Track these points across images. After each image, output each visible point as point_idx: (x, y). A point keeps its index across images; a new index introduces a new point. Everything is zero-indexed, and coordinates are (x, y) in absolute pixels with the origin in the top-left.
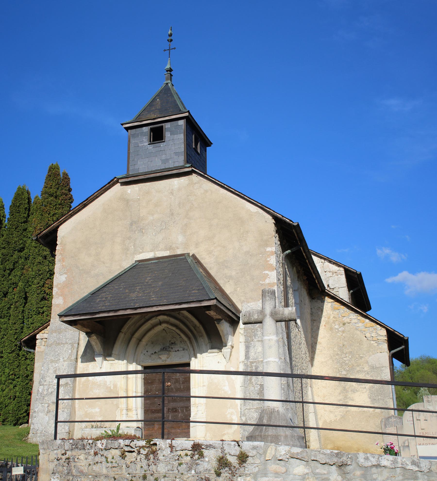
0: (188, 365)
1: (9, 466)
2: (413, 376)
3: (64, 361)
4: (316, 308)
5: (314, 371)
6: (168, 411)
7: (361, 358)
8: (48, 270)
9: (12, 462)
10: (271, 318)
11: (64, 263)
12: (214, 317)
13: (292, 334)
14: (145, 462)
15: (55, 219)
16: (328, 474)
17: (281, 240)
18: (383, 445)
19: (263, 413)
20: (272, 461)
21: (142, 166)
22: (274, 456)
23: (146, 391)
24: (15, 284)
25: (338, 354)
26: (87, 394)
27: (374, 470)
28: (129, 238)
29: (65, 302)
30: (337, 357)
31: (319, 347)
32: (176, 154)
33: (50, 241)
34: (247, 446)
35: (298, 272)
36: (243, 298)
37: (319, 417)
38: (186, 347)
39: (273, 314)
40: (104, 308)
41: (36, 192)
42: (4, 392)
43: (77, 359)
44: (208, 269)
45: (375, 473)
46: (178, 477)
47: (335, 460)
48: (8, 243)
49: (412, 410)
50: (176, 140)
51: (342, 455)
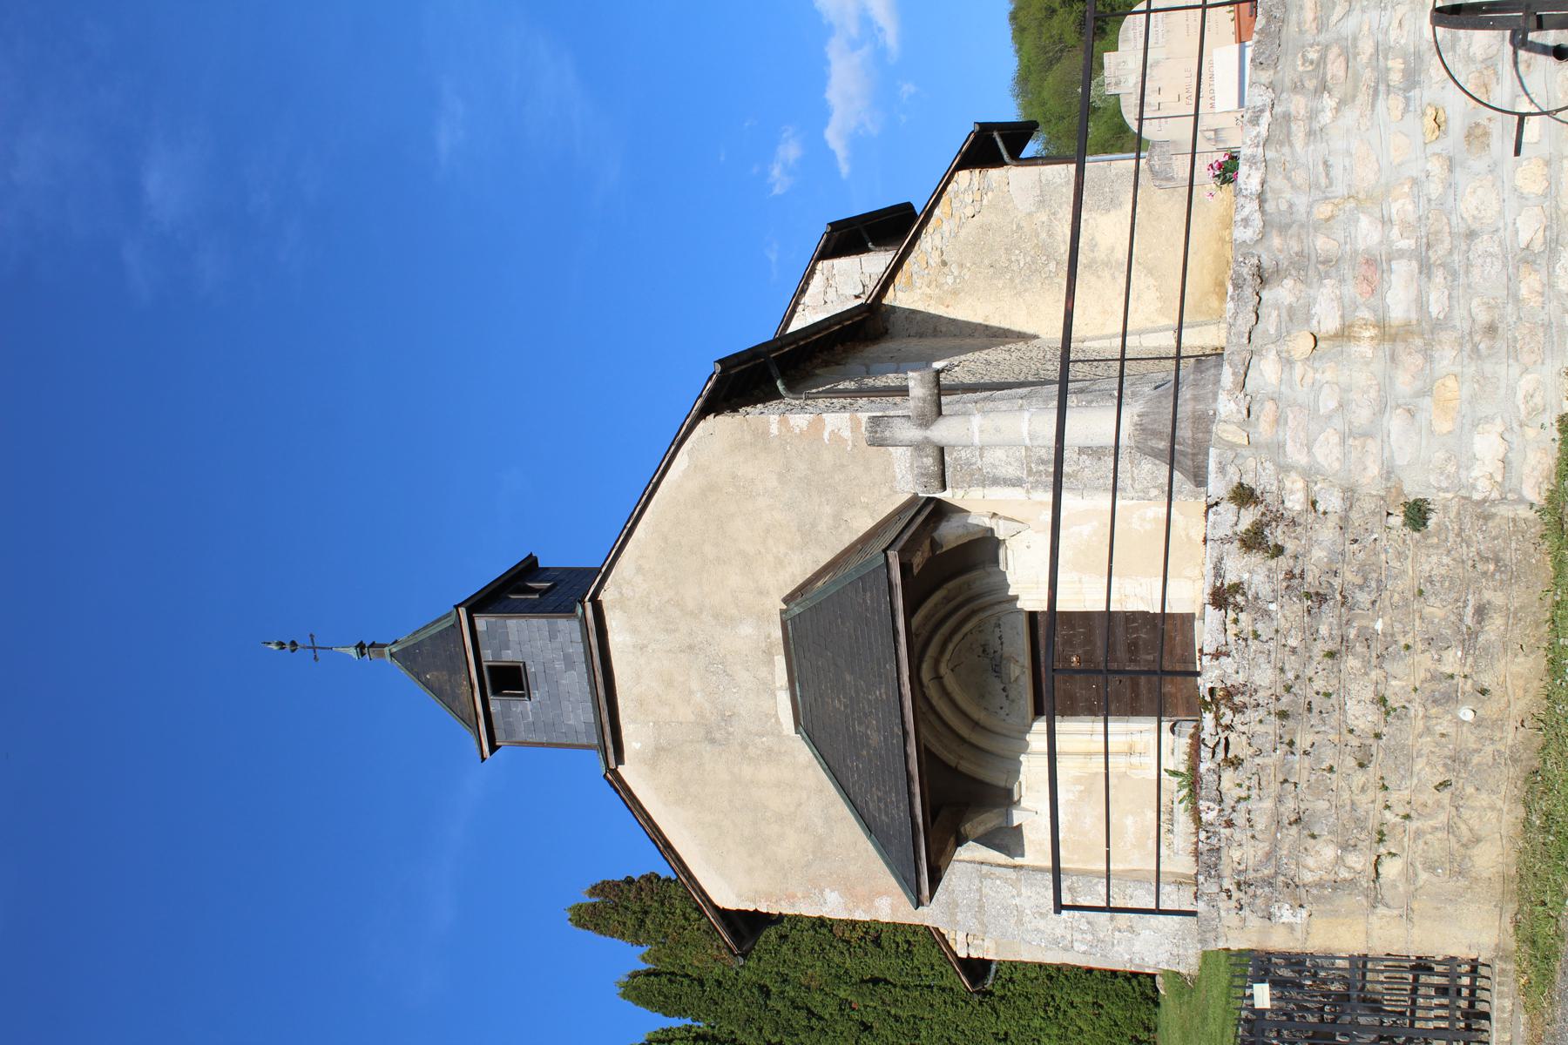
0: (1032, 616)
1: (1251, 1016)
2: (1059, 120)
3: (1019, 895)
5: (1052, 332)
6: (1134, 661)
7: (1019, 227)
8: (812, 932)
9: (1241, 1009)
12: (926, 555)
13: (966, 381)
14: (1251, 714)
15: (695, 915)
17: (753, 401)
18: (1212, 185)
19: (1144, 450)
21: (579, 715)
22: (1240, 425)
23: (1091, 711)
24: (843, 1004)
25: (1012, 279)
26: (1093, 844)
27: (1270, 207)
29: (886, 893)
31: (995, 321)
32: (552, 636)
33: (747, 926)
34: (1218, 486)
35: (826, 364)
36: (885, 490)
37: (1149, 325)
38: (993, 621)
39: (925, 421)
40: (904, 806)
41: (630, 957)
42: (1085, 1028)
43: (1015, 867)
47: (1248, 291)
48: (749, 1020)
49: (1141, 120)
50: (522, 637)
51: (1239, 275)
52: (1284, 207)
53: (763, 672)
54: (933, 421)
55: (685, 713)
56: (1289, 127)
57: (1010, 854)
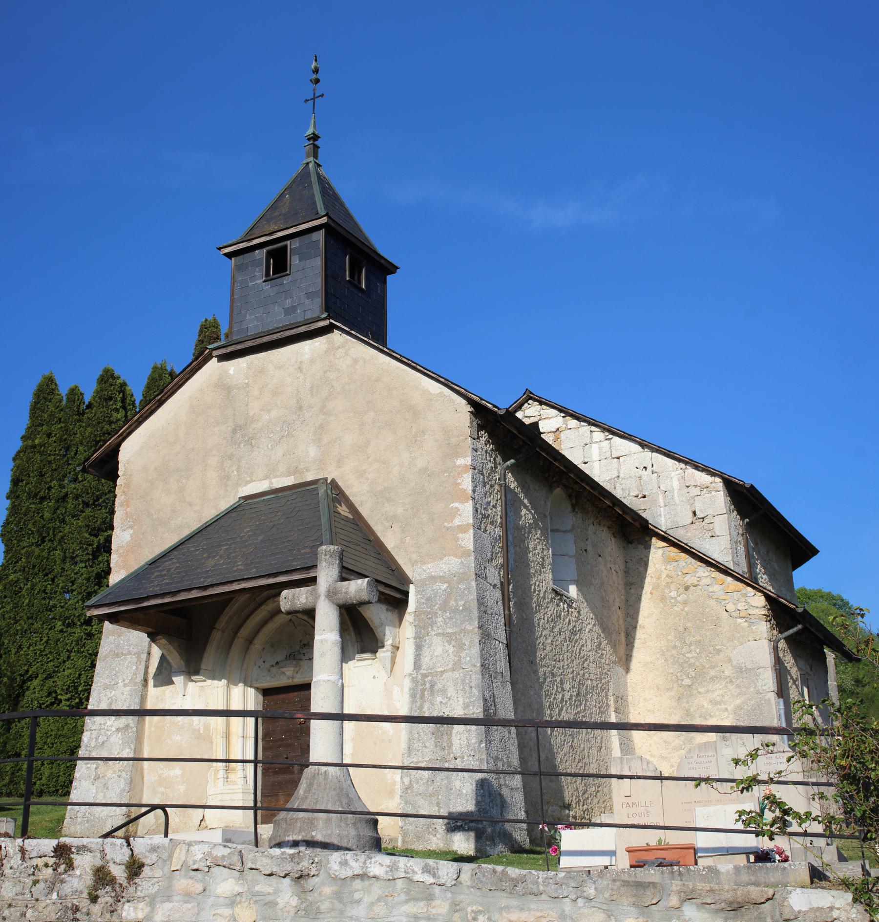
3: (125, 685)
4: (634, 560)
7: (719, 651)
10: (327, 600)
11: (128, 510)
16: (275, 893)
20: (182, 872)
21: (254, 323)
25: (675, 647)
27: (358, 884)
28: (231, 457)
30: (674, 652)
31: (640, 634)
32: (309, 295)
33: (108, 468)
36: (415, 556)
40: (158, 590)
43: (146, 680)
44: (357, 506)
45: (358, 890)
46: (30, 906)
47: (288, 867)
50: (308, 270)
52: (357, 896)
53: (282, 468)
54: (332, 601)
55: (254, 408)
56: (422, 900)
57: (156, 675)
